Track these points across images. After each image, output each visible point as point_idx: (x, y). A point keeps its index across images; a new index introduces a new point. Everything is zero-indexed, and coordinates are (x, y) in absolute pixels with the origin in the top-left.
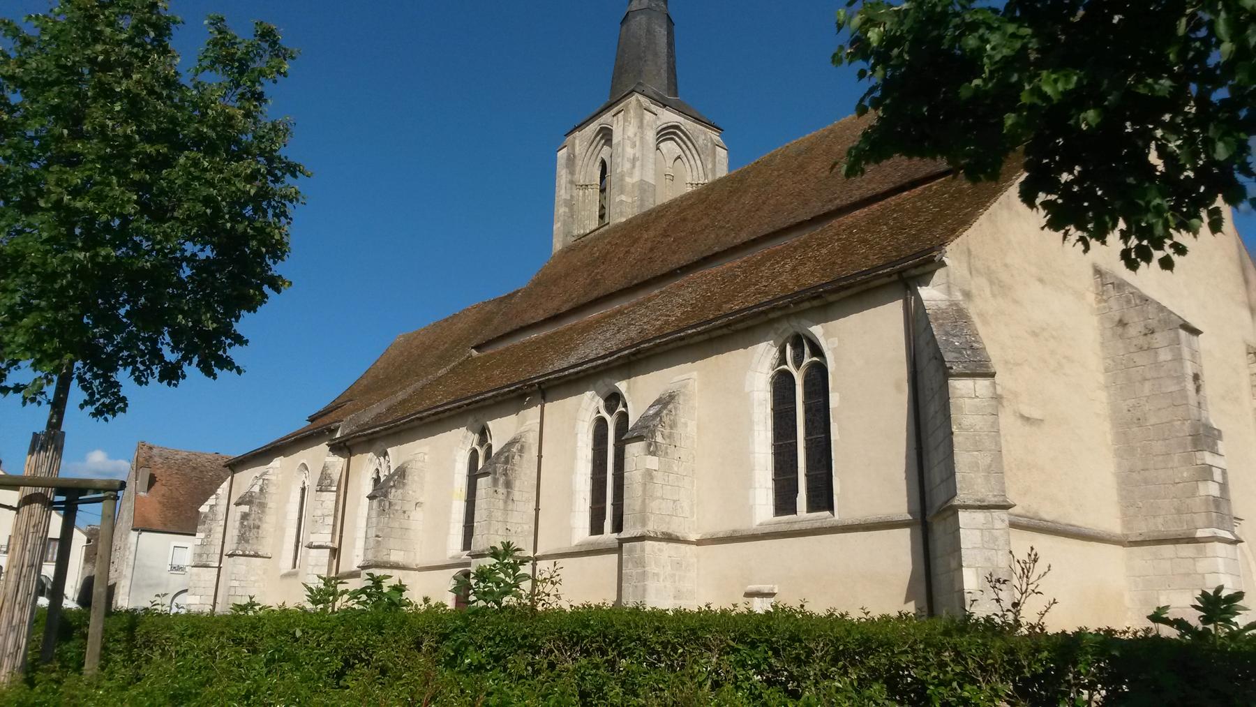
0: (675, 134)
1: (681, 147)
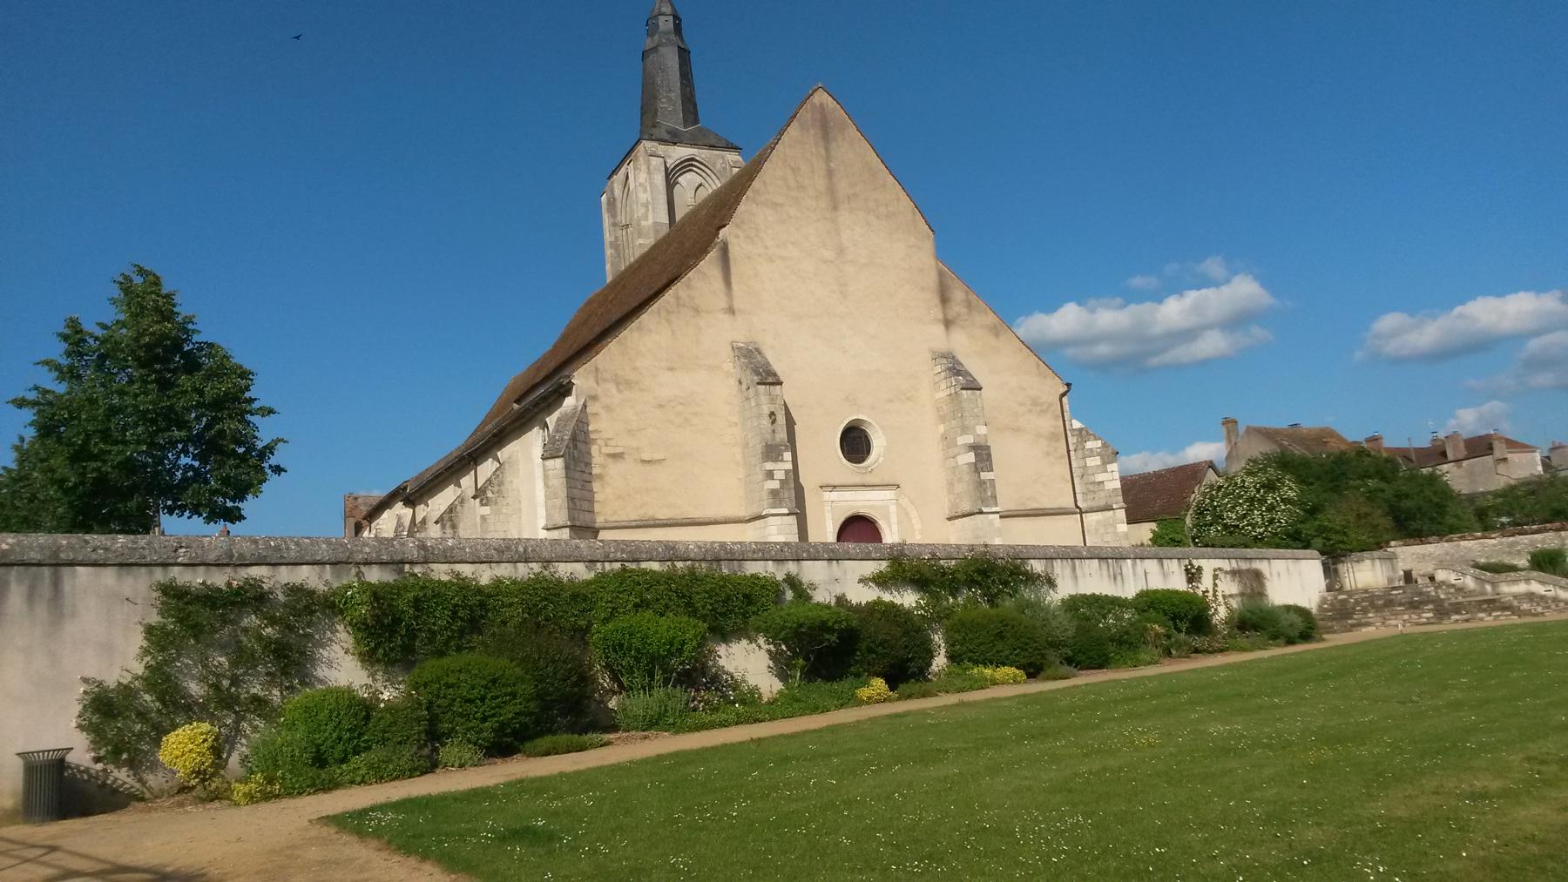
0: (692, 165)
1: (701, 176)
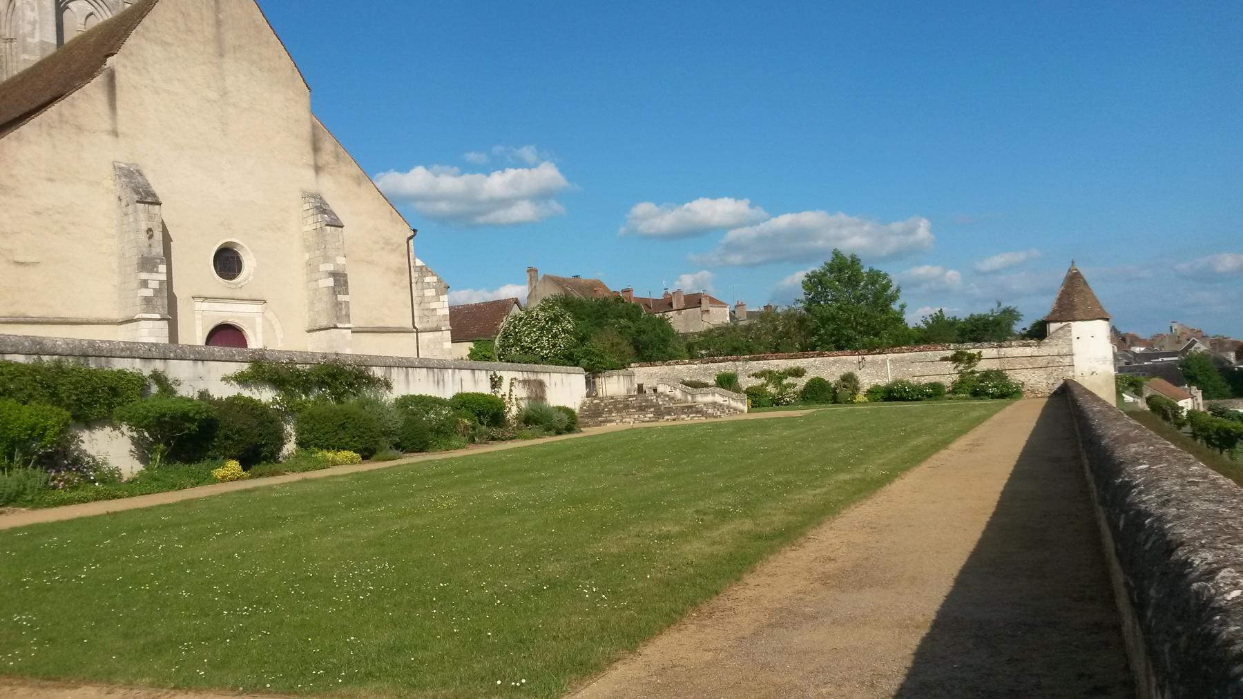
1: (92, 4)
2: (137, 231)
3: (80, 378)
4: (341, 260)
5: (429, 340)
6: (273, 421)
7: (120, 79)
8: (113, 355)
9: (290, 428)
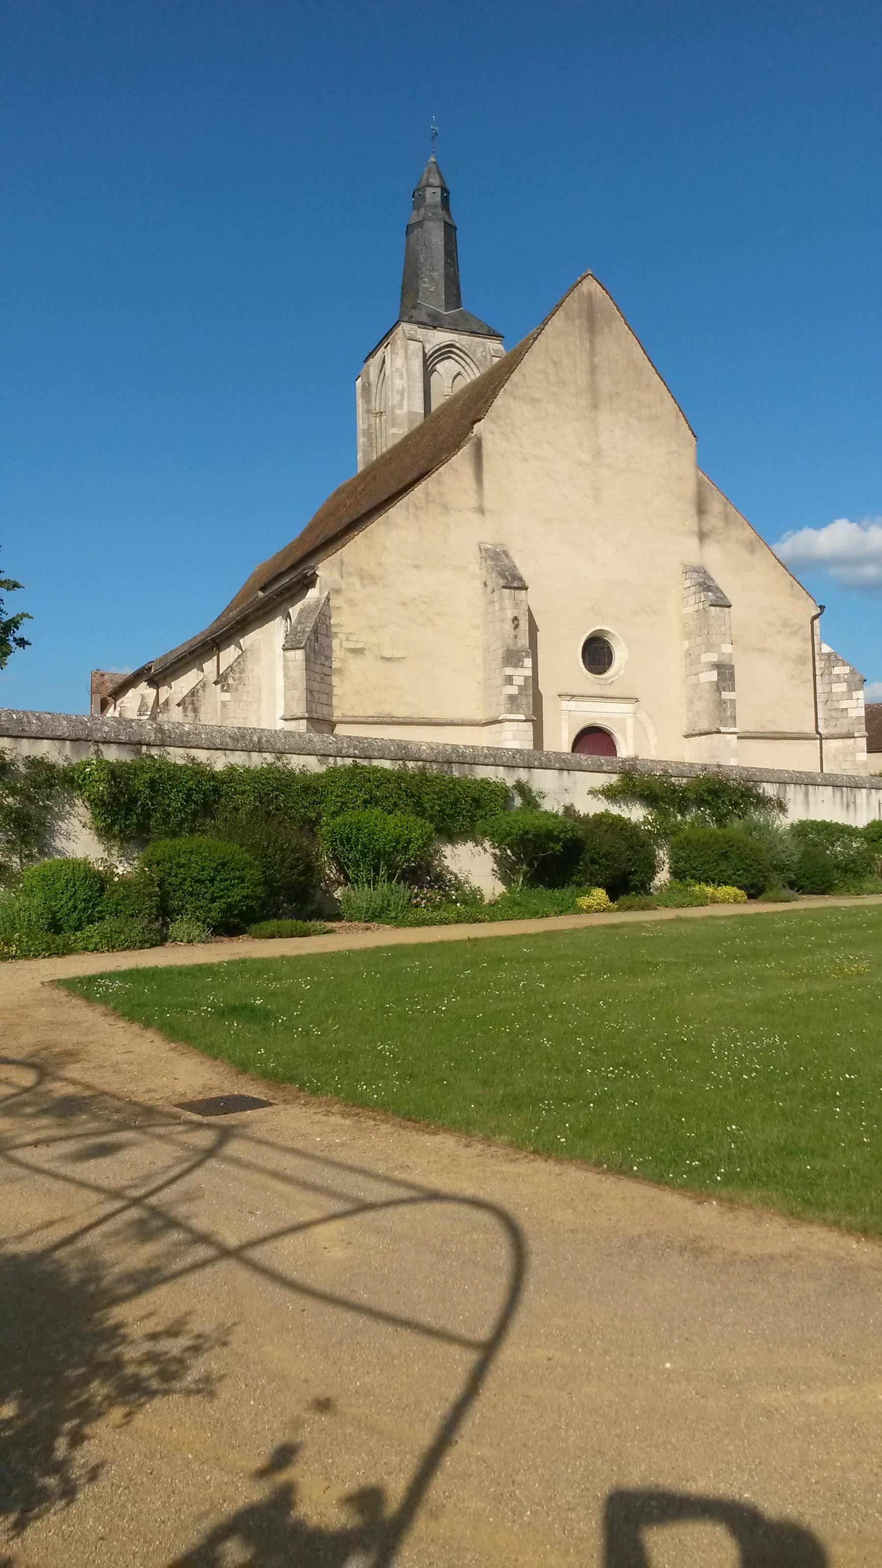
1: (459, 363)
2: (503, 620)
3: (444, 787)
4: (727, 649)
5: (837, 749)
6: (644, 845)
7: (488, 447)
8: (476, 762)
9: (662, 854)
